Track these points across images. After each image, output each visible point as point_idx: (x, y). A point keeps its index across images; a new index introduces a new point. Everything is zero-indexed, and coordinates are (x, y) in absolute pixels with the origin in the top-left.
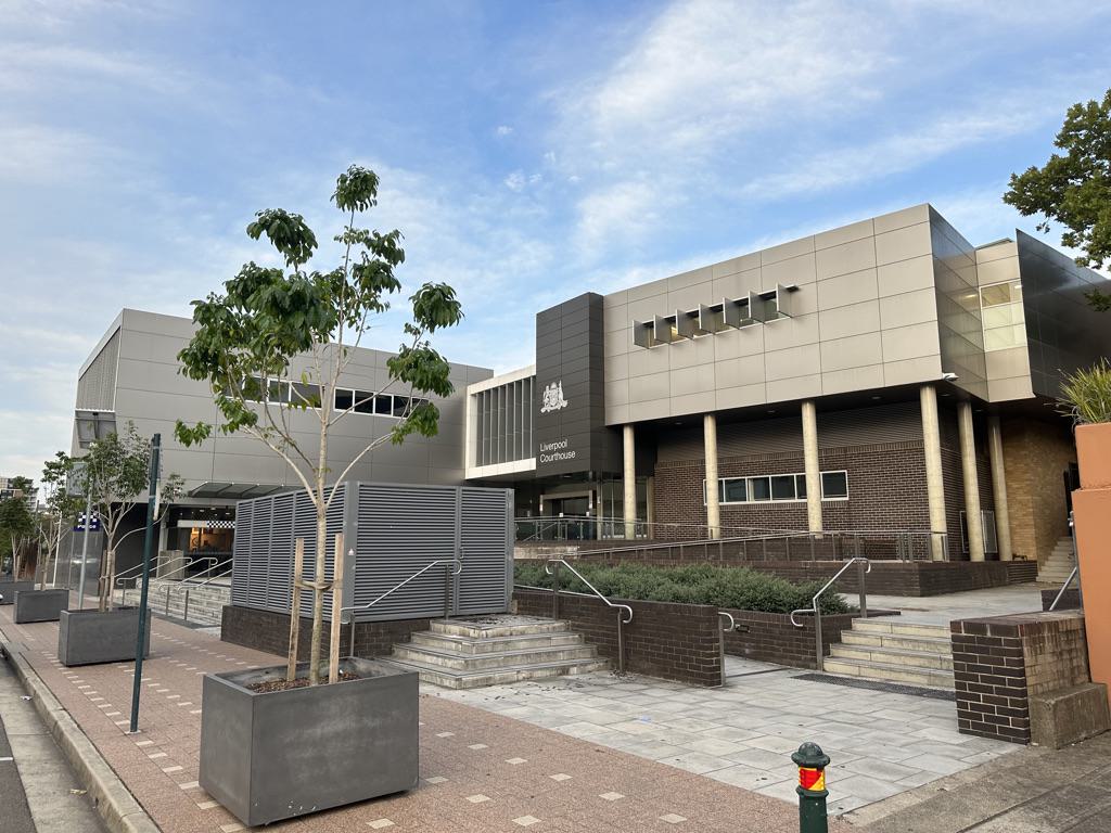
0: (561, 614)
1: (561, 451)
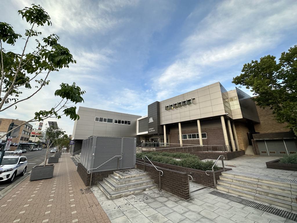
0: (146, 170)
1: (152, 130)
